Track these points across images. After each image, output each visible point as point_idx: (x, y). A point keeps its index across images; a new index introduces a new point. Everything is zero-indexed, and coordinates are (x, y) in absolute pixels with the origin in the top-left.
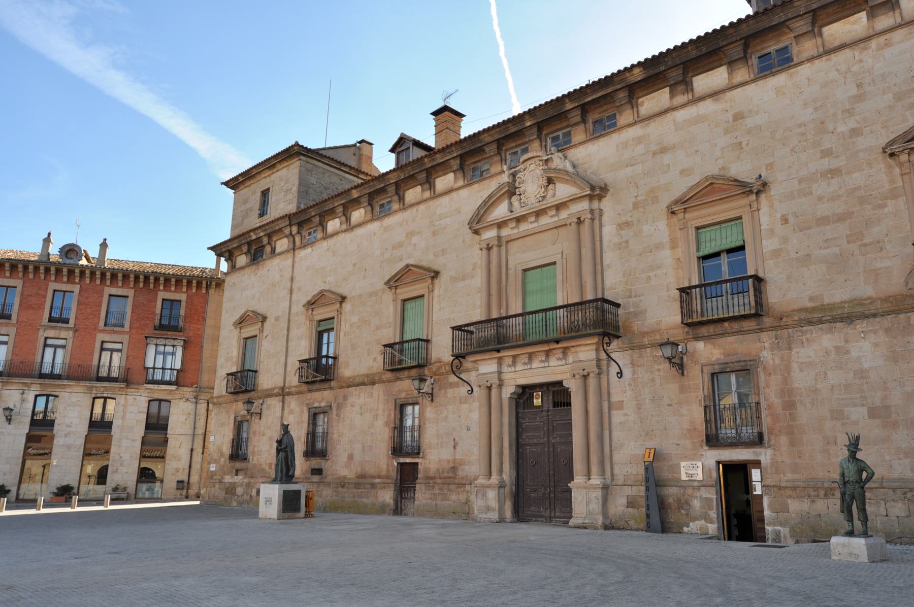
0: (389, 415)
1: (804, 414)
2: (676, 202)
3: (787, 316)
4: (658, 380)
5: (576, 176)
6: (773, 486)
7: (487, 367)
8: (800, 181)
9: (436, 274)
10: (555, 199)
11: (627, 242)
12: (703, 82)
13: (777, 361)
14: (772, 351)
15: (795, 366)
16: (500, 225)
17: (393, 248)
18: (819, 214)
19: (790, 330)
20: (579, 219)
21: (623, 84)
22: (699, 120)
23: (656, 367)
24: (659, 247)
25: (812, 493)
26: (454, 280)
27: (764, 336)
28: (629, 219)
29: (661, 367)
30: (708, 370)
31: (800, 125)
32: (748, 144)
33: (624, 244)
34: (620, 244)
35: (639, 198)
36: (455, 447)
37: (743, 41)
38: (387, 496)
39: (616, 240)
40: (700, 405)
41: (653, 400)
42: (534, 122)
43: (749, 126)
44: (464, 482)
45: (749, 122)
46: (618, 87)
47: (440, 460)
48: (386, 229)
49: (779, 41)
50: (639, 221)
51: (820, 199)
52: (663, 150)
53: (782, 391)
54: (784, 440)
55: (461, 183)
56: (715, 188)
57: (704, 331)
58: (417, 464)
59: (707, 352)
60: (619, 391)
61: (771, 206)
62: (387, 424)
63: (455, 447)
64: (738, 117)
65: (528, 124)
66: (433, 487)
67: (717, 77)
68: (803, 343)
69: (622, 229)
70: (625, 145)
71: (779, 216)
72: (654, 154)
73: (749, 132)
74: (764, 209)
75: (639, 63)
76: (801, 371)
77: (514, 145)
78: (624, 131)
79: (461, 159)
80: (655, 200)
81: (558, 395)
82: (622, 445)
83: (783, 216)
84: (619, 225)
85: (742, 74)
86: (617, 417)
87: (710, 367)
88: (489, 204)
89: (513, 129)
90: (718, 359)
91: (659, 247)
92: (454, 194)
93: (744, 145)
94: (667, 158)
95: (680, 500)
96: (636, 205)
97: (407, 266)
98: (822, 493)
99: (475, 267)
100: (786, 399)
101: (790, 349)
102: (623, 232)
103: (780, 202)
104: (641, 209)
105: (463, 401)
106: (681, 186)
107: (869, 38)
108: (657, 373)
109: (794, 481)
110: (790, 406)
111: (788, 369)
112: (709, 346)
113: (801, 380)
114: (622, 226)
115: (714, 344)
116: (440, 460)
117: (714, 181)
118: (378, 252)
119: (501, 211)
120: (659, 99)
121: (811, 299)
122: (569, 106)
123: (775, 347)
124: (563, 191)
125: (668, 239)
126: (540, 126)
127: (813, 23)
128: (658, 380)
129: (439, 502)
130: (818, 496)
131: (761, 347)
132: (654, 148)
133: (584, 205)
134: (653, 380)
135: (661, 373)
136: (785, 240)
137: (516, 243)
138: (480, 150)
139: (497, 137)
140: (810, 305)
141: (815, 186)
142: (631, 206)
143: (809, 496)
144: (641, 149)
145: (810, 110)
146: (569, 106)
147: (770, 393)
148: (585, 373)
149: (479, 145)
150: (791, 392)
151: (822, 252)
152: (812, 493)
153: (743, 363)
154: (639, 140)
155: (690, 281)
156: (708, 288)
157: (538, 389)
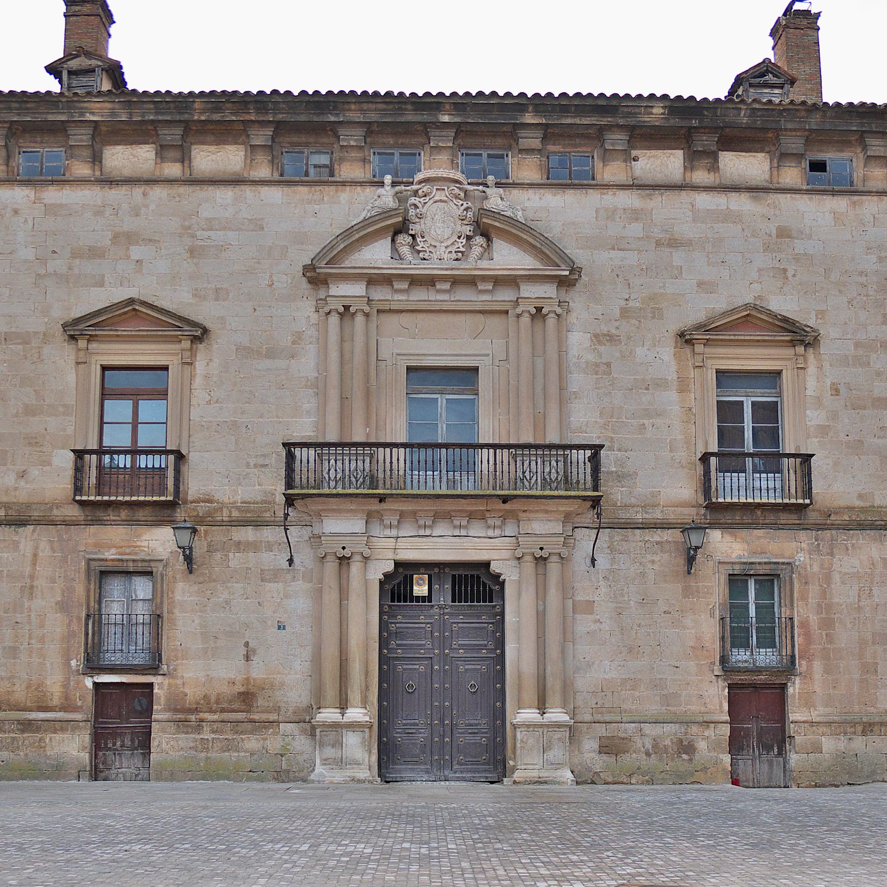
0: (69, 591)
1: (845, 637)
2: (699, 327)
3: (836, 513)
4: (651, 576)
5: (521, 233)
6: (804, 722)
7: (342, 525)
8: (857, 345)
9: (200, 334)
10: (484, 264)
11: (608, 365)
12: (209, 158)
13: (816, 568)
14: (810, 554)
15: (836, 577)
16: (374, 280)
17: (76, 254)
18: (876, 393)
19: (833, 532)
20: (539, 309)
21: (631, 121)
22: (728, 217)
23: (649, 557)
24: (660, 384)
25: (849, 730)
26: (246, 352)
27: (802, 535)
28: (614, 331)
29: (656, 558)
30: (725, 570)
31: (861, 274)
32: (794, 276)
33: (603, 368)
34: (597, 365)
35: (631, 304)
36: (247, 658)
37: (7, 125)
38: (74, 746)
39: (590, 357)
40: (712, 615)
41: (642, 603)
42: (457, 120)
43: (797, 251)
44: (273, 717)
45: (799, 246)
46: (621, 122)
47: (210, 679)
48: (50, 210)
49: (842, 151)
50: (629, 338)
51: (878, 374)
52: (674, 243)
53: (819, 605)
54: (818, 666)
55: (264, 171)
56: (751, 321)
57: (727, 518)
58: (150, 685)
59: (727, 547)
60: (590, 587)
61: (820, 368)
62: (63, 607)
63: (247, 658)
64: (783, 233)
65: (446, 118)
66: (198, 729)
67: (226, 158)
68: (847, 549)
69: (600, 343)
70: (611, 214)
71: (828, 383)
72: (658, 243)
73: (797, 259)
74: (812, 369)
75: (665, 97)
76: (843, 583)
77: (391, 141)
78: (610, 192)
79: (276, 129)
80: (657, 314)
81: (475, 584)
82: (589, 665)
83: (833, 384)
84: (596, 336)
85: (792, 175)
86: (583, 624)
87: (729, 567)
88: (357, 236)
89: (410, 117)
90: (740, 557)
91: (660, 384)
92: (248, 191)
93: (790, 274)
94: (678, 257)
95: (681, 741)
96: (625, 313)
97: (131, 301)
98: (859, 729)
99: (298, 338)
100: (824, 616)
101: (832, 554)
102: (602, 348)
103: (831, 365)
104: (633, 321)
105: (276, 575)
106: (698, 309)
107: (766, 190)
108: (650, 566)
109: (829, 715)
110: (827, 624)
111: (828, 578)
112: (728, 538)
113: (843, 595)
114: (598, 338)
115: (736, 537)
116: (210, 679)
117: (754, 313)
118: (27, 253)
119: (377, 255)
120: (669, 163)
121: (860, 496)
122: (529, 118)
123: (816, 550)
124: (507, 257)
125: (675, 376)
126: (460, 130)
127: (183, 137)
128: (651, 576)
129: (212, 755)
130: (855, 733)
131: (790, 547)
132: (657, 233)
133: (549, 290)
134: (643, 574)
135: (656, 567)
136: (834, 415)
137: (394, 319)
138: (425, 130)
139: (373, 117)
140: (858, 503)
141: (874, 356)
142: (618, 313)
143: (845, 734)
144: (636, 229)
145: (873, 258)
146: (529, 118)
147: (803, 610)
148: (544, 554)
149: (332, 119)
150: (829, 607)
151: (876, 440)
152: (849, 730)
153: (772, 566)
154: (635, 215)
155: (368, 435)
156: (450, 451)
157: (422, 570)
